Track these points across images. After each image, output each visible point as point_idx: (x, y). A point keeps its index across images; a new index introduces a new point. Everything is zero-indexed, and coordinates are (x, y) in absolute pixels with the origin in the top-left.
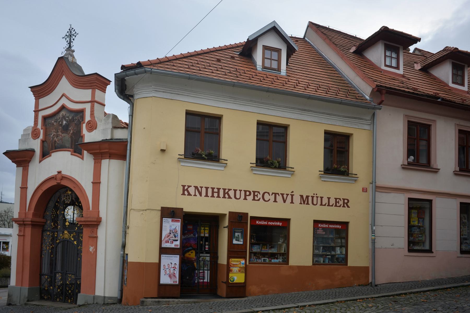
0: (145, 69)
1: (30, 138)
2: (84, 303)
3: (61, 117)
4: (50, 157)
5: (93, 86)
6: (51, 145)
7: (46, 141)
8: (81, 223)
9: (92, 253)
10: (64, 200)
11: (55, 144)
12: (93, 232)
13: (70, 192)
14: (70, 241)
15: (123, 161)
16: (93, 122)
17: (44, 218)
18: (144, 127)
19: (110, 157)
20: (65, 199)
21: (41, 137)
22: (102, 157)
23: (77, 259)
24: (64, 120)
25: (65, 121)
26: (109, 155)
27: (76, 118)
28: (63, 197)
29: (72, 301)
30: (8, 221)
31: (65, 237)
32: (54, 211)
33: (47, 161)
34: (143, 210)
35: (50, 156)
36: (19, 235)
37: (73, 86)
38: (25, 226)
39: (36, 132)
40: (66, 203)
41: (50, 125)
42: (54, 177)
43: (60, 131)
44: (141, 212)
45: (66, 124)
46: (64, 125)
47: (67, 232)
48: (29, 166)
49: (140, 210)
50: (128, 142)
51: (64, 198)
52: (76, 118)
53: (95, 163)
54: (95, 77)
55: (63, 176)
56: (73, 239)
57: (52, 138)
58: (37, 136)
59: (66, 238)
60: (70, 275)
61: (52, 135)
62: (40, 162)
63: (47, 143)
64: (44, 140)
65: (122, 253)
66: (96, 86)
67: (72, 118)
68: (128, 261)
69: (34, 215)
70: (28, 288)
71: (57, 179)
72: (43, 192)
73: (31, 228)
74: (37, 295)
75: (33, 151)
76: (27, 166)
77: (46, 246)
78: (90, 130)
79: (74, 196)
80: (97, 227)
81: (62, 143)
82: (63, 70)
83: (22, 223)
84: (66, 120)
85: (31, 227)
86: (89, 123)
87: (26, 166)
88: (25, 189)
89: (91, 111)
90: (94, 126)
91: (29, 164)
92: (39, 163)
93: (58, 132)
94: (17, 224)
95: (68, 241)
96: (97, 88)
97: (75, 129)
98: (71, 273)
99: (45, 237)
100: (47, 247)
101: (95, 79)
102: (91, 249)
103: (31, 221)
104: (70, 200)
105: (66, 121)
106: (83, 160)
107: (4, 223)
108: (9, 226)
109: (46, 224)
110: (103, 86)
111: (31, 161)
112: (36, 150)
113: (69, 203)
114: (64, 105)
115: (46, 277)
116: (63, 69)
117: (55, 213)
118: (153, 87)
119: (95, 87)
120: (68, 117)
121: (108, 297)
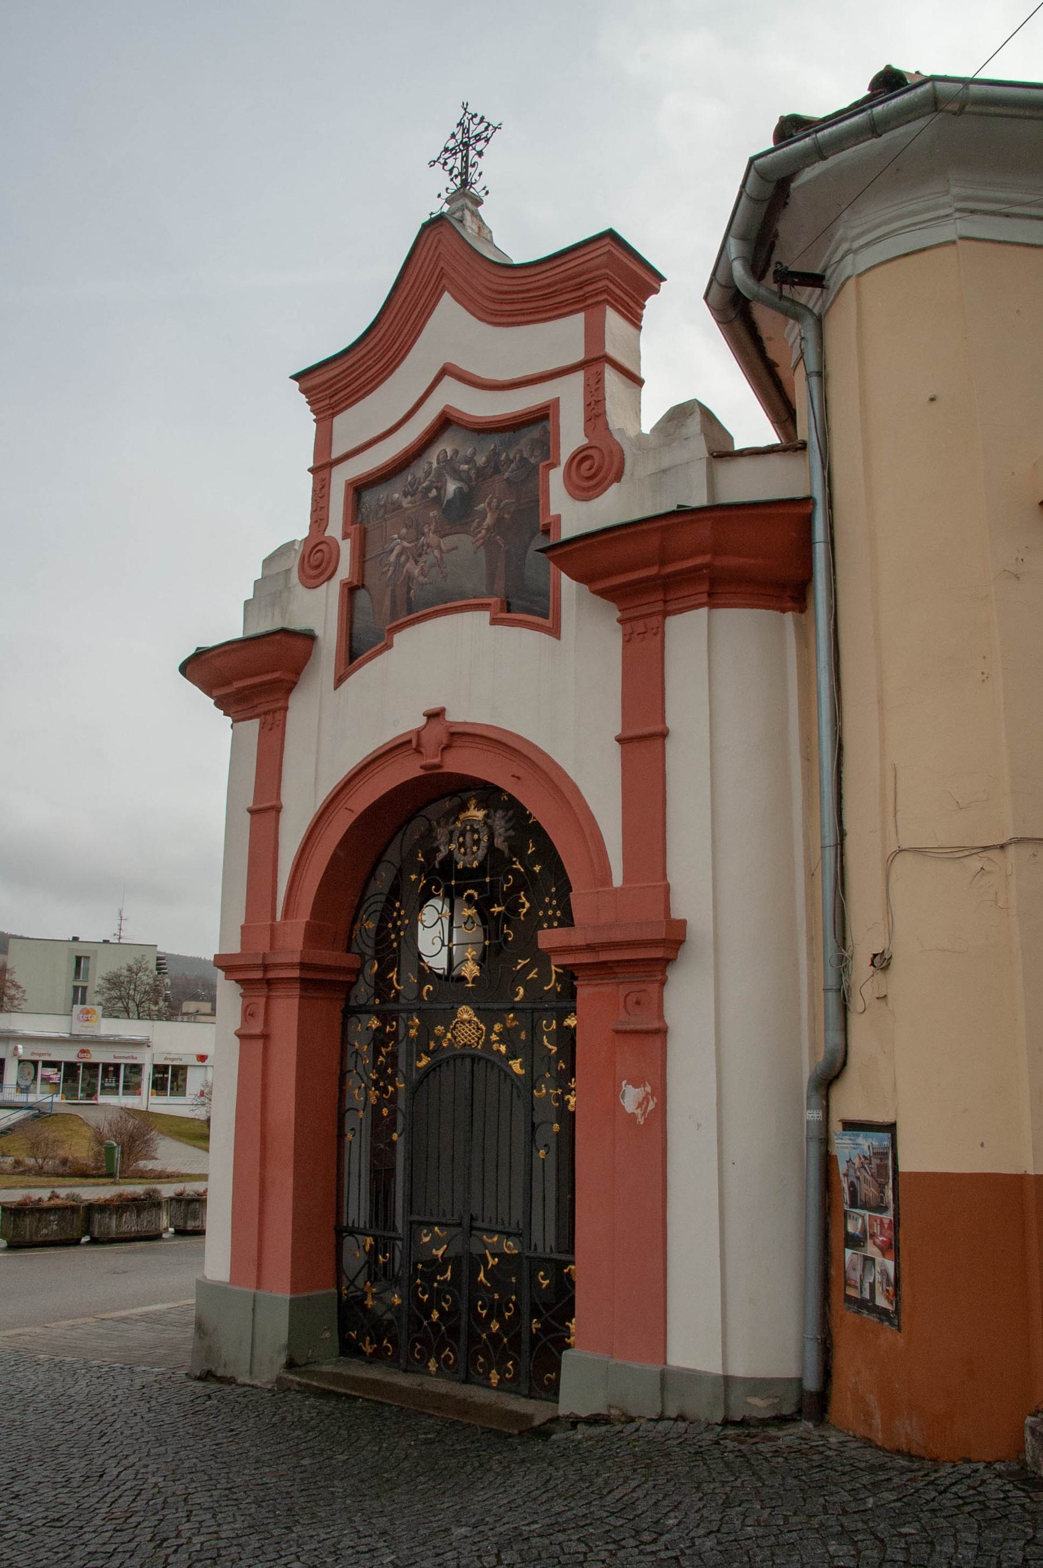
0: (934, 88)
1: (295, 586)
2: (605, 1412)
3: (438, 469)
4: (386, 653)
5: (592, 296)
6: (387, 602)
7: (363, 586)
8: (569, 960)
9: (641, 1121)
10: (451, 852)
11: (409, 589)
12: (638, 1003)
13: (478, 810)
14: (487, 1061)
15: (777, 613)
16: (600, 450)
17: (348, 950)
18: (930, 395)
19: (710, 595)
20: (453, 846)
21: (344, 571)
22: (665, 602)
23: (530, 1156)
24: (448, 477)
25: (455, 479)
26: (705, 587)
27: (511, 457)
28: (442, 839)
29: (509, 1380)
30: (138, 997)
31: (462, 1040)
32: (402, 912)
33: (369, 672)
34: (986, 848)
35: (389, 646)
36: (241, 1036)
37: (490, 323)
38: (270, 990)
39: (319, 554)
40: (460, 866)
41: (381, 513)
42: (410, 742)
43: (432, 527)
44: (975, 863)
45: (459, 492)
46: (448, 501)
47: (471, 1012)
48: (286, 709)
49: (965, 848)
50: (814, 504)
51: (450, 842)
52: (511, 457)
53: (627, 640)
54: (606, 249)
55: (453, 730)
56: (503, 1048)
57: (391, 568)
58: (326, 569)
59: (465, 1045)
60: (495, 1239)
61: (395, 553)
62: (339, 681)
63: (370, 595)
64: (356, 583)
65: (814, 1115)
66: (606, 290)
67: (488, 461)
68: (903, 1168)
69: (313, 934)
70: (291, 1300)
71: (422, 750)
72: (355, 817)
73: (301, 997)
74: (327, 1335)
75: (309, 637)
76: (280, 709)
77: (365, 1088)
78: (584, 489)
79: (502, 830)
80: (663, 972)
81: (445, 577)
82: (442, 268)
83: (258, 975)
84: (457, 475)
85: (297, 992)
86: (580, 457)
87: (274, 711)
88: (273, 813)
89: (588, 405)
90: (612, 463)
91: (287, 699)
92: (335, 689)
93: (423, 534)
94: (237, 981)
95: (475, 1059)
96: (613, 301)
97: (507, 504)
98: (500, 1228)
99: (356, 1044)
100: (367, 1094)
101: (604, 258)
102: (631, 1098)
103: (303, 966)
104: (481, 853)
105: (461, 480)
106: (559, 638)
107: (127, 1004)
108: (139, 1014)
109: (361, 977)
110: (632, 297)
111: (295, 683)
112: (318, 632)
113: (475, 864)
114: (448, 410)
115: (370, 1240)
116: (441, 264)
117: (541, 913)
118: (955, 190)
119: (600, 298)
120: (469, 461)
121: (744, 1380)
